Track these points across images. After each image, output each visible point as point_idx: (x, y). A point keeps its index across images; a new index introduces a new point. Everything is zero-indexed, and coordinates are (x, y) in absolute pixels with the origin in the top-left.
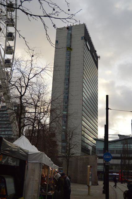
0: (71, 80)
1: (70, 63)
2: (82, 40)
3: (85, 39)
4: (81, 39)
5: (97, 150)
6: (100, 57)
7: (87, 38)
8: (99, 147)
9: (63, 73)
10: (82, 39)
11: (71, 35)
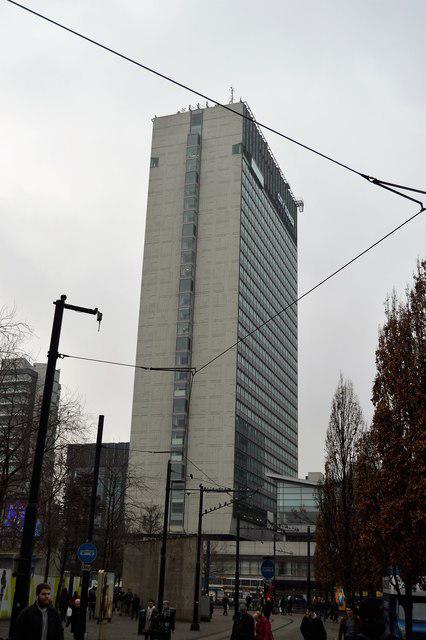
0: (199, 286)
1: (195, 229)
2: (236, 156)
3: (244, 151)
4: (231, 152)
5: (283, 513)
6: (302, 204)
7: (253, 146)
8: (287, 504)
9: (172, 261)
10: (235, 151)
11: (200, 139)
